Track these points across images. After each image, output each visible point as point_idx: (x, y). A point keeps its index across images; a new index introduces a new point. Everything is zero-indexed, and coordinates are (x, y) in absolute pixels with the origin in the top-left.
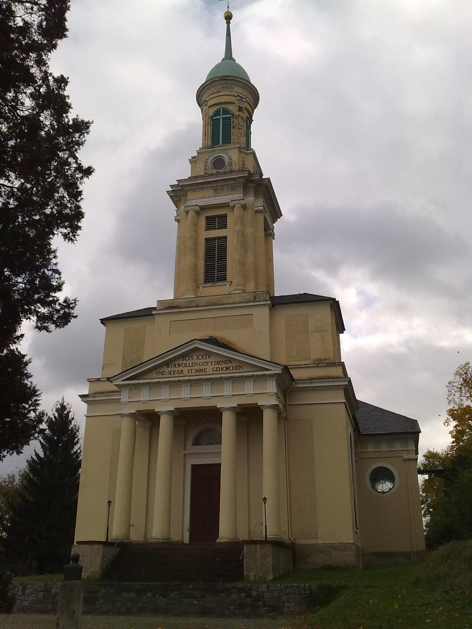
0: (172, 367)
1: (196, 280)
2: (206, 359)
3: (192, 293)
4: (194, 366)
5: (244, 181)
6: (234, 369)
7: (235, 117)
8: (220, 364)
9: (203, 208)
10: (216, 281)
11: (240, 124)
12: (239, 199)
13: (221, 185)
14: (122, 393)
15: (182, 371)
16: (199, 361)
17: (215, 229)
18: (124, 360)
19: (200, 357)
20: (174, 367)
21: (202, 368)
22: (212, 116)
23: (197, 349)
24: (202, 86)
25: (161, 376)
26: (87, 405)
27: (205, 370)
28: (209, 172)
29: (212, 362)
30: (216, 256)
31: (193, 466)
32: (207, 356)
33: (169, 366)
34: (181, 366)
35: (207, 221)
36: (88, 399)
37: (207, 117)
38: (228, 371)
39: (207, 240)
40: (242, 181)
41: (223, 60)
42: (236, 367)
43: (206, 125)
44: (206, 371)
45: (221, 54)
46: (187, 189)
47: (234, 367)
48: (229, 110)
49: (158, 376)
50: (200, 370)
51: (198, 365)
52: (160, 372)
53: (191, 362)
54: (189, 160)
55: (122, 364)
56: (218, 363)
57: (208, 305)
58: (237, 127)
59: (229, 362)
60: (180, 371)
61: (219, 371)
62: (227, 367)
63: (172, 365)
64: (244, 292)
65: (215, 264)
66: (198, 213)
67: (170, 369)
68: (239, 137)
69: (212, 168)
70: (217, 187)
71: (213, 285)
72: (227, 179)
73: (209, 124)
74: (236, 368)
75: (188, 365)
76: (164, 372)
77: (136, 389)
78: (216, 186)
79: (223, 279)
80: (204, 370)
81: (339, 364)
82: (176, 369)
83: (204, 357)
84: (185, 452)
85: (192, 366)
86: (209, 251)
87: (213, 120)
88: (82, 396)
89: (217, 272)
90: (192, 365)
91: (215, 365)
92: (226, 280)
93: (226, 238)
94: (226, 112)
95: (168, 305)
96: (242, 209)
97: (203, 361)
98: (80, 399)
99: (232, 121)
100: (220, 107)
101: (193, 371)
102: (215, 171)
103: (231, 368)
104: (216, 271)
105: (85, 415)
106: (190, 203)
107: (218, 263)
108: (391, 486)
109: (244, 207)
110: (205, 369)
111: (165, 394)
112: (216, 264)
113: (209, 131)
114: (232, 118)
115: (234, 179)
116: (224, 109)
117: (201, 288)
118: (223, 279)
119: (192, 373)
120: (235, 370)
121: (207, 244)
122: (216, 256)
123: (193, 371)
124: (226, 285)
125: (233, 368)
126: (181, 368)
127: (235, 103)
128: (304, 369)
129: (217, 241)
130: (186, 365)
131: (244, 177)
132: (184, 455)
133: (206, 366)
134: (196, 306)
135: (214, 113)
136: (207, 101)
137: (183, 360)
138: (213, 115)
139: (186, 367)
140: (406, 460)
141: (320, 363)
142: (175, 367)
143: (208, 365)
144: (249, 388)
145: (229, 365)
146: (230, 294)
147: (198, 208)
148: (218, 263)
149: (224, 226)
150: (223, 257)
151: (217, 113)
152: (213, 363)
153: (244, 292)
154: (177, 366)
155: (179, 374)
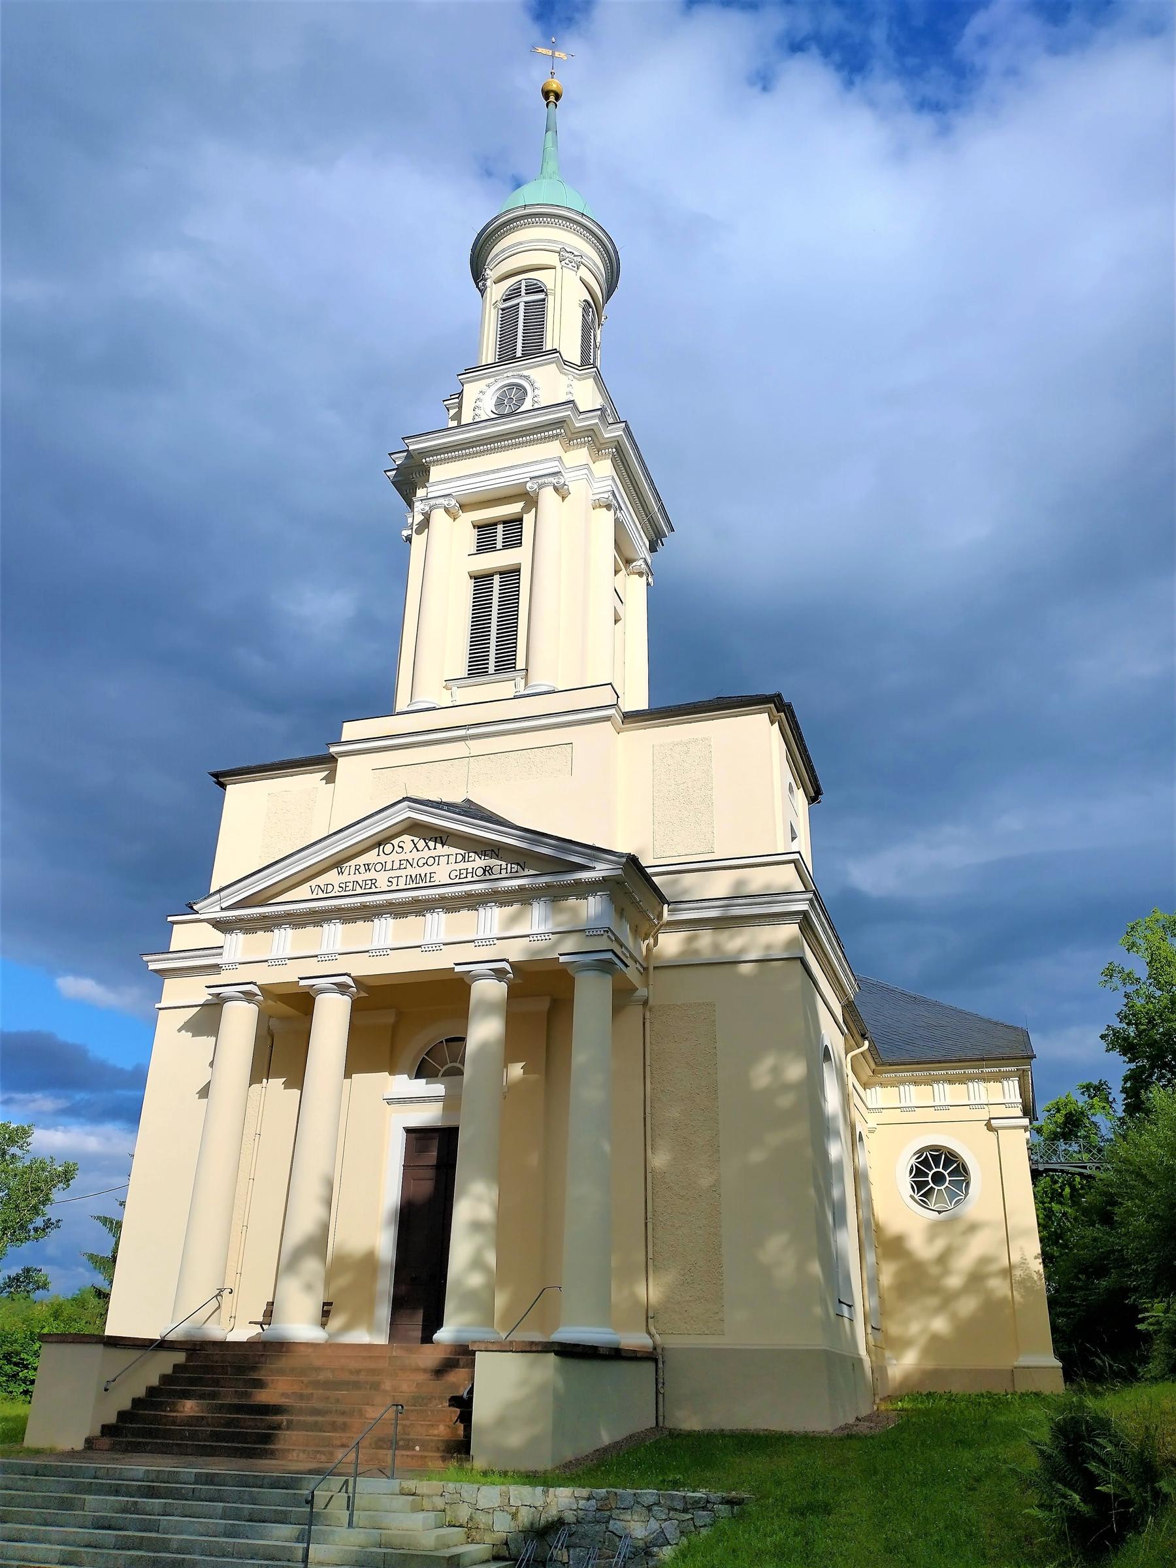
15: (373, 882)
50: (418, 876)
53: (395, 857)
75: (389, 866)
126: (372, 875)
133: (434, 868)
149: (513, 541)
154: (362, 870)
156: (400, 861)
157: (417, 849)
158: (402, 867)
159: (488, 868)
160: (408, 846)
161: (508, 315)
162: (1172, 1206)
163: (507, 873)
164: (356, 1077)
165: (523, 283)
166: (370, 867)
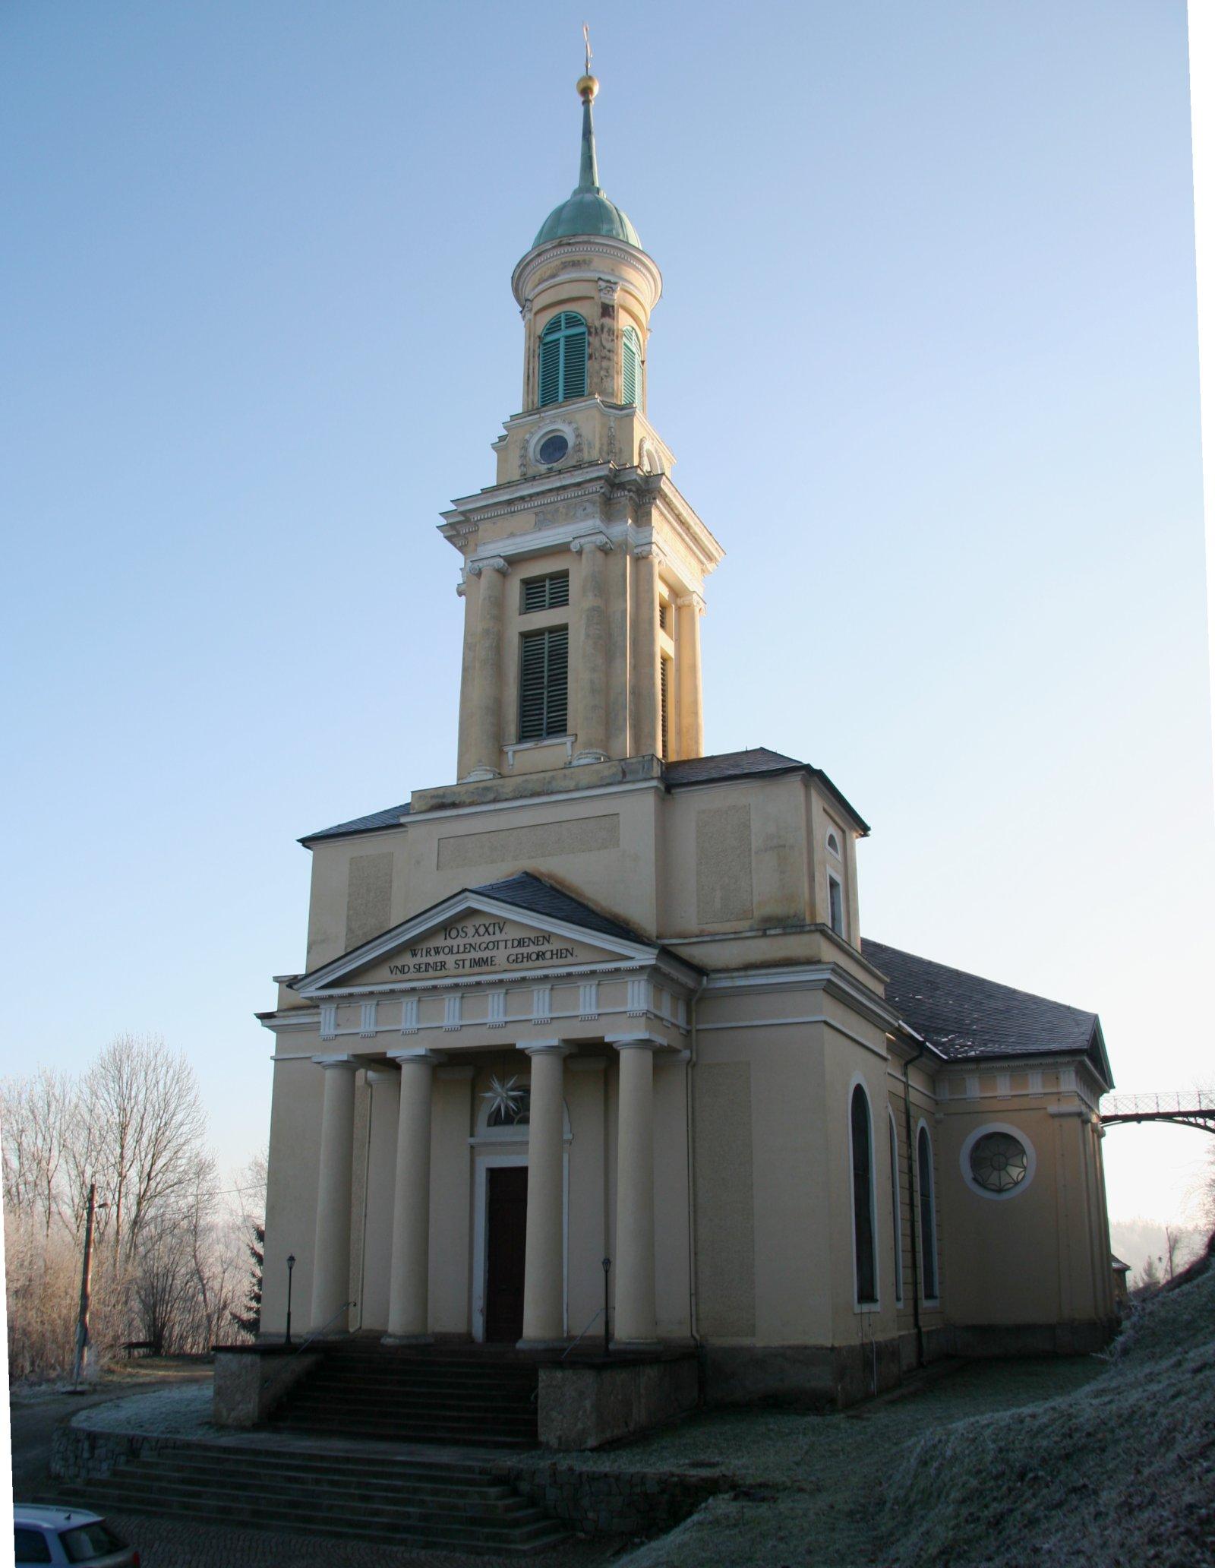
0: (422, 956)
3: (488, 768)
4: (469, 952)
5: (601, 488)
6: (555, 956)
7: (593, 330)
9: (513, 561)
10: (544, 735)
11: (604, 348)
12: (593, 532)
13: (551, 503)
14: (323, 1012)
15: (443, 965)
16: (477, 940)
17: (542, 607)
18: (350, 930)
20: (426, 956)
21: (485, 954)
23: (472, 913)
24: (518, 265)
25: (400, 976)
26: (275, 1034)
28: (531, 472)
29: (506, 941)
30: (546, 675)
35: (528, 589)
36: (274, 1022)
37: (532, 339)
38: (541, 963)
39: (525, 636)
41: (575, 193)
42: (559, 953)
44: (493, 963)
45: (574, 181)
46: (476, 519)
47: (555, 952)
48: (580, 317)
49: (393, 977)
53: (460, 941)
55: (347, 939)
56: (519, 943)
57: (522, 797)
58: (597, 355)
60: (439, 964)
62: (539, 952)
65: (543, 693)
66: (502, 573)
67: (418, 960)
68: (602, 379)
69: (537, 461)
70: (543, 507)
71: (537, 745)
72: (564, 488)
74: (558, 954)
75: (455, 950)
78: (541, 505)
79: (558, 728)
81: (813, 928)
82: (431, 959)
84: (472, 1140)
85: (464, 952)
86: (535, 661)
89: (549, 713)
91: (513, 947)
92: (565, 730)
93: (564, 628)
94: (573, 321)
96: (600, 555)
97: (487, 938)
98: (260, 1023)
101: (467, 963)
102: (543, 468)
103: (548, 955)
104: (545, 711)
105: (272, 1058)
107: (549, 692)
108: (1019, 1174)
112: (546, 693)
115: (579, 484)
116: (569, 315)
117: (510, 754)
118: (558, 728)
119: (463, 967)
121: (527, 645)
122: (546, 675)
123: (467, 963)
126: (441, 957)
127: (593, 298)
128: (732, 943)
130: (451, 951)
131: (599, 478)
132: (472, 1147)
133: (494, 952)
134: (495, 801)
135: (547, 327)
136: (531, 301)
137: (446, 939)
139: (452, 953)
140: (1053, 1116)
141: (769, 929)
143: (498, 948)
144: (586, 1001)
145: (542, 948)
146: (568, 765)
147: (501, 562)
148: (549, 692)
149: (560, 599)
150: (559, 678)
151: (554, 326)
152: (509, 944)
154: (433, 952)
157: (485, 926)
159: (541, 953)
160: (471, 931)
165: (563, 316)
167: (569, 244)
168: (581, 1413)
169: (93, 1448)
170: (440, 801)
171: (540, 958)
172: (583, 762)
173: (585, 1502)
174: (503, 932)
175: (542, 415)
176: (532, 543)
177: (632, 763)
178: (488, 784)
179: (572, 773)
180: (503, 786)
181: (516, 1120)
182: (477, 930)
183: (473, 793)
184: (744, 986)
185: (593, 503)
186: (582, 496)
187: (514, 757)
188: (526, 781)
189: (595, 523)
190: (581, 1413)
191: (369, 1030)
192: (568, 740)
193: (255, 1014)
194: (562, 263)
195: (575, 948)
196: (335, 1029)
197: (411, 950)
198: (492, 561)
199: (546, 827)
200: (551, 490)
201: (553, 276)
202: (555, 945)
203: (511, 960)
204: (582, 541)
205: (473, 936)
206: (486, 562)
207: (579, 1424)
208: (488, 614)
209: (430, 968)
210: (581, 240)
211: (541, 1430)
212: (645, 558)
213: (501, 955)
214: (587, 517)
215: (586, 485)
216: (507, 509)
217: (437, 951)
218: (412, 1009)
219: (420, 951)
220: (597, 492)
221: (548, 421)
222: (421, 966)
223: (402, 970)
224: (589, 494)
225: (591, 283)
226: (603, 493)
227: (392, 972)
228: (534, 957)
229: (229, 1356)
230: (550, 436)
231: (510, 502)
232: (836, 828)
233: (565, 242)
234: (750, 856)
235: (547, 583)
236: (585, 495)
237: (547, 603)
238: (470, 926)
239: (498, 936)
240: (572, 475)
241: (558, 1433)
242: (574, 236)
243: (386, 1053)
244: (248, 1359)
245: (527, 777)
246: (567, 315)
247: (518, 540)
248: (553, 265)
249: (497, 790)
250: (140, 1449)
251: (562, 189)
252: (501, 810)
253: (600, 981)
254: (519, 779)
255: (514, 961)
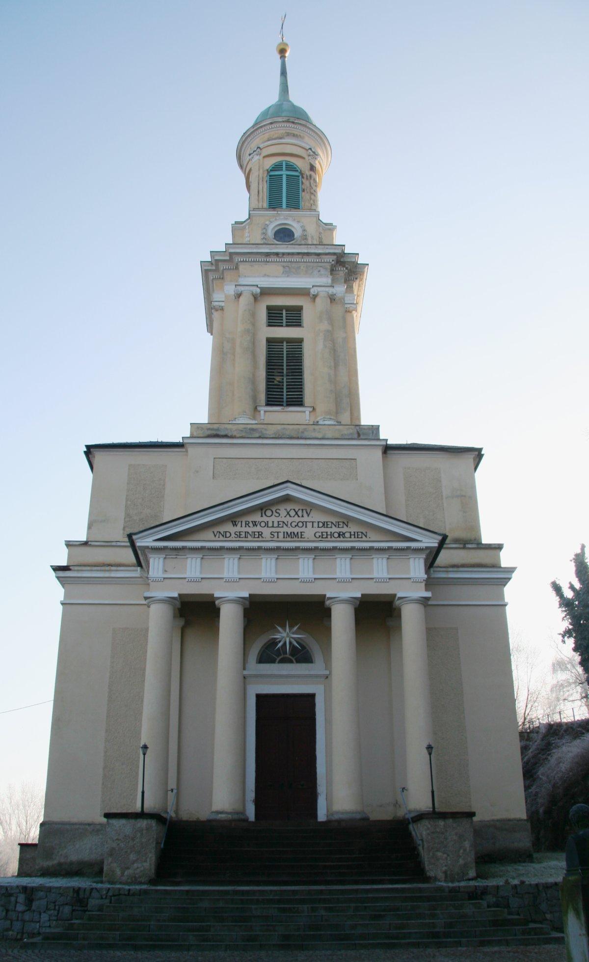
1: (254, 399)
2: (303, 516)
8: (327, 527)
9: (266, 292)
13: (296, 262)
15: (260, 534)
16: (290, 520)
18: (128, 515)
19: (292, 513)
21: (296, 530)
22: (269, 170)
23: (287, 499)
27: (301, 535)
31: (259, 697)
32: (304, 511)
33: (237, 523)
34: (259, 525)
37: (261, 171)
39: (270, 341)
40: (331, 261)
43: (259, 180)
50: (292, 533)
51: (289, 525)
52: (220, 532)
53: (273, 518)
54: (232, 224)
55: (125, 522)
56: (324, 525)
59: (344, 525)
61: (327, 537)
63: (242, 522)
64: (339, 424)
66: (256, 298)
67: (238, 528)
70: (290, 263)
71: (284, 409)
72: (308, 254)
73: (265, 180)
74: (356, 535)
76: (227, 533)
77: (176, 558)
79: (297, 401)
80: (299, 534)
82: (250, 530)
83: (298, 513)
85: (278, 527)
87: (270, 176)
88: (57, 569)
90: (279, 524)
91: (318, 527)
94: (290, 167)
95: (209, 432)
97: (296, 519)
99: (301, 182)
100: (283, 160)
101: (281, 535)
106: (242, 281)
109: (332, 299)
110: (301, 532)
111: (230, 567)
113: (265, 190)
114: (300, 177)
115: (318, 255)
117: (262, 412)
118: (297, 401)
119: (278, 537)
120: (355, 537)
123: (281, 535)
124: (305, 412)
125: (351, 535)
126: (258, 529)
129: (285, 344)
130: (267, 524)
131: (334, 254)
138: (271, 169)
139: (268, 527)
142: (247, 525)
143: (306, 527)
144: (379, 568)
151: (277, 167)
152: (316, 525)
153: (339, 424)
154: (251, 524)
155: (254, 537)
156: (278, 522)
158: (280, 526)
160: (283, 513)
161: (273, 195)
162: (586, 606)
163: (355, 537)
164: (19, 846)
166: (257, 523)
167: (293, 123)
168: (462, 851)
169: (29, 901)
170: (215, 432)
171: (341, 536)
172: (327, 422)
173: (544, 906)
174: (310, 516)
175: (279, 212)
176: (281, 283)
177: (364, 429)
178: (254, 427)
179: (320, 429)
180: (266, 430)
181: (277, 661)
182: (288, 513)
183: (242, 431)
184: (455, 578)
185: (326, 269)
186: (319, 262)
187: (264, 415)
188: (284, 429)
189: (328, 280)
190: (462, 851)
191: (191, 576)
192: (308, 410)
193: (51, 566)
194: (286, 132)
195: (368, 532)
196: (163, 573)
197: (232, 521)
198: (251, 288)
199: (300, 460)
200: (299, 254)
201: (281, 138)
202: (353, 528)
203: (317, 535)
204: (319, 289)
205: (285, 517)
206: (247, 288)
207: (460, 860)
208: (249, 320)
209: (249, 536)
210: (301, 123)
211: (427, 866)
212: (350, 312)
213: (309, 532)
214: (321, 276)
215: (323, 256)
216: (263, 259)
217: (255, 524)
218: (234, 564)
219: (240, 523)
220: (330, 262)
221: (282, 217)
222: (241, 533)
223: (224, 535)
224: (324, 262)
225: (304, 150)
226: (332, 264)
227: (215, 536)
228: (336, 535)
229: (123, 821)
230: (283, 227)
231: (268, 255)
232: (132, 572)
233: (291, 120)
234: (442, 499)
235: (284, 312)
236: (321, 262)
237: (284, 324)
238: (283, 509)
239: (306, 519)
240: (316, 247)
241: (444, 868)
242: (298, 118)
243: (213, 594)
244: (143, 823)
245: (285, 426)
246: (286, 163)
247: (271, 279)
248: (282, 131)
249: (261, 431)
250: (88, 899)
251: (273, 98)
252: (267, 444)
253: (389, 556)
254: (279, 427)
255: (320, 536)
